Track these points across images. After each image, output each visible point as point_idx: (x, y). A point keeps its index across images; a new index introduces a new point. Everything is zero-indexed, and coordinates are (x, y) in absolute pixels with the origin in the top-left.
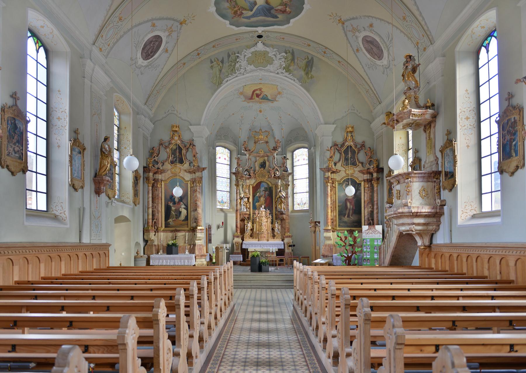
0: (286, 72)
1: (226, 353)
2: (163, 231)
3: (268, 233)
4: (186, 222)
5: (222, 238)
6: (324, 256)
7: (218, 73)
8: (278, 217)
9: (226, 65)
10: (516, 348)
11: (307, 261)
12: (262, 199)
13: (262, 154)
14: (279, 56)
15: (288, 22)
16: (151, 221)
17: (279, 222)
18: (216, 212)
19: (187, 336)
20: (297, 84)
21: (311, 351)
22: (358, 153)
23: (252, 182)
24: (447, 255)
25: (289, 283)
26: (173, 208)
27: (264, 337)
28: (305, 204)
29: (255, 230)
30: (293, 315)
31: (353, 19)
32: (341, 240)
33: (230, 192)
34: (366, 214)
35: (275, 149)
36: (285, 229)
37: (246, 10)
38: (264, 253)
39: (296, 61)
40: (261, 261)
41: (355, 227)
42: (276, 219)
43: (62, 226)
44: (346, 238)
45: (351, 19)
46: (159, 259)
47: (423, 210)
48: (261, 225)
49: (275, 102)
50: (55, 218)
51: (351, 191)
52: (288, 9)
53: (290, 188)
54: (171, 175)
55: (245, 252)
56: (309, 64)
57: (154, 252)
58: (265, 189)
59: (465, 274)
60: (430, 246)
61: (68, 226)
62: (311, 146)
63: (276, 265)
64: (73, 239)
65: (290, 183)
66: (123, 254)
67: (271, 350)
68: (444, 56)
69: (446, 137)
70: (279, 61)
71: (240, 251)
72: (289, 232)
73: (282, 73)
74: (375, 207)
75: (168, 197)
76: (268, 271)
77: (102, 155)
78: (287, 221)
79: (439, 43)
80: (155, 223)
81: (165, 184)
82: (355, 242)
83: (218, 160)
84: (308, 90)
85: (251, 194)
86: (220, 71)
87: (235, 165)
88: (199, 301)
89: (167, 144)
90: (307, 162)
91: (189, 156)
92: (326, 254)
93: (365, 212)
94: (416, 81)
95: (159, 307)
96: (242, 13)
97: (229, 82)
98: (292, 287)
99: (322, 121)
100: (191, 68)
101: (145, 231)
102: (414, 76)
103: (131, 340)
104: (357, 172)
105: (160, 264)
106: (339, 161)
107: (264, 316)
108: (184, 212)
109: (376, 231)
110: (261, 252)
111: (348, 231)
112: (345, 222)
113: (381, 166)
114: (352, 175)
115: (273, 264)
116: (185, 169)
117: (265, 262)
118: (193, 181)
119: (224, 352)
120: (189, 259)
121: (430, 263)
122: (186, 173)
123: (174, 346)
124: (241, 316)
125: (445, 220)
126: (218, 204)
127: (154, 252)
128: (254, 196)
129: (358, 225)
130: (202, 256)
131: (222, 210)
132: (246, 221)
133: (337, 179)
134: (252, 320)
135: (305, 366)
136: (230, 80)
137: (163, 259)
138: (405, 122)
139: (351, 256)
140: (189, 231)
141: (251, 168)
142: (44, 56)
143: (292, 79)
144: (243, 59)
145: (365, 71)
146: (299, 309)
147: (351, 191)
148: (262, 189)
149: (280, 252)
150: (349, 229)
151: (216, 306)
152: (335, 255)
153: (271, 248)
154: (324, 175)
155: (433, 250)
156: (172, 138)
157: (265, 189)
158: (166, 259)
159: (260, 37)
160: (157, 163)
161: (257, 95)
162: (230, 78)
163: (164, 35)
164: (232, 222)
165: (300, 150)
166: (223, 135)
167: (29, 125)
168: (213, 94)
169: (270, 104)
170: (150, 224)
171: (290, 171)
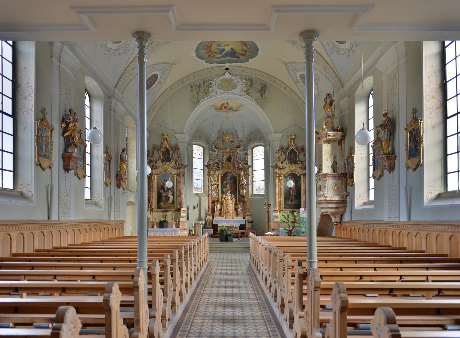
0: (246, 94)
1: (194, 321)
2: (157, 211)
3: (233, 213)
4: (172, 205)
5: (197, 216)
6: (273, 230)
7: (196, 95)
8: (240, 199)
9: (202, 89)
10: (363, 277)
11: (261, 232)
13: (228, 150)
14: (241, 83)
15: (248, 61)
17: (242, 204)
19: (172, 289)
20: (255, 103)
21: (276, 329)
22: (299, 154)
23: (220, 173)
24: (349, 229)
25: (247, 250)
26: (163, 195)
27: (229, 300)
29: (223, 210)
30: (248, 267)
31: (293, 63)
32: (285, 218)
33: (203, 180)
35: (238, 147)
37: (217, 53)
38: (229, 228)
39: (253, 86)
41: (297, 208)
42: (239, 201)
43: (101, 209)
44: (288, 216)
45: (291, 63)
46: (154, 231)
47: (334, 199)
49: (238, 112)
50: (96, 204)
51: (291, 184)
52: (247, 53)
55: (215, 227)
56: (263, 89)
57: (150, 226)
58: (230, 174)
59: (390, 246)
60: (340, 223)
61: (103, 209)
62: (266, 145)
63: (238, 237)
64: (106, 218)
65: (250, 174)
66: (130, 228)
67: (235, 310)
68: (349, 96)
70: (241, 86)
71: (211, 226)
72: (249, 211)
75: (160, 187)
77: (121, 161)
78: (247, 203)
79: (347, 87)
80: (150, 205)
81: (158, 177)
82: (295, 219)
83: (194, 156)
84: (262, 108)
85: (220, 182)
86: (198, 93)
87: (207, 159)
88: (172, 271)
89: (159, 148)
90: (263, 157)
91: (175, 156)
92: (275, 228)
94: (332, 111)
95: (139, 276)
96: (215, 56)
97: (204, 102)
98: (248, 252)
99: (273, 131)
102: (331, 108)
103: (115, 304)
104: (298, 168)
107: (229, 283)
110: (228, 227)
112: (289, 205)
115: (237, 236)
118: (178, 175)
119: (193, 320)
120: (176, 231)
121: (341, 235)
122: (172, 169)
123: (151, 309)
124: (214, 268)
125: (348, 204)
126: (194, 189)
128: (222, 184)
129: (298, 207)
130: (184, 229)
133: (283, 174)
134: (219, 287)
135: (266, 333)
137: (157, 231)
138: (324, 139)
139: (292, 229)
140: (175, 211)
141: (220, 161)
142: (89, 100)
146: (252, 263)
147: (291, 184)
148: (229, 178)
149: (242, 227)
150: (292, 210)
151: (187, 275)
154: (274, 171)
155: (342, 225)
156: (163, 143)
157: (230, 174)
158: (159, 231)
159: (227, 69)
161: (224, 107)
162: (205, 99)
163: (158, 73)
164: (205, 204)
166: (198, 136)
167: (86, 148)
169: (235, 113)
171: (250, 164)
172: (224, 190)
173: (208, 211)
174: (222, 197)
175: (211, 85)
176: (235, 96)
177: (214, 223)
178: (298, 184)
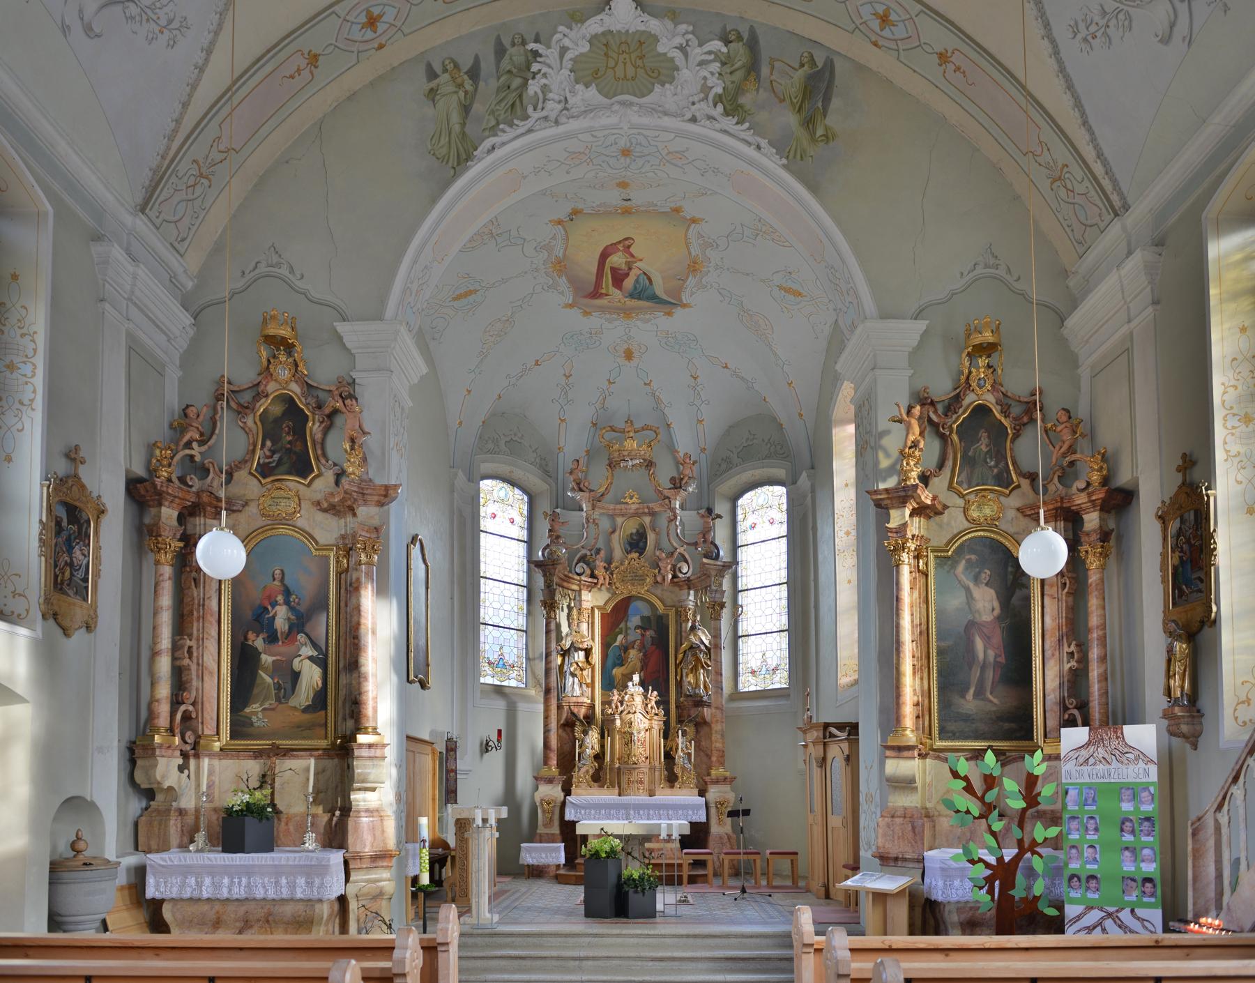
0: (727, 113)
3: (652, 769)
7: (455, 118)
8: (684, 713)
9: (489, 85)
12: (634, 655)
13: (633, 504)
14: (697, 53)
16: (164, 709)
17: (690, 730)
18: (478, 694)
20: (772, 162)
22: (1017, 436)
26: (266, 659)
28: (775, 670)
29: (608, 758)
34: (1053, 683)
36: (709, 757)
39: (765, 71)
40: (625, 873)
48: (628, 739)
49: (678, 312)
53: (726, 614)
54: (261, 521)
56: (818, 86)
65: (727, 599)
69: (1178, 478)
70: (698, 70)
71: (556, 830)
72: (722, 764)
73: (710, 118)
74: (1094, 653)
75: (248, 614)
76: (650, 913)
78: (717, 727)
80: (186, 717)
83: (485, 524)
84: (814, 188)
86: (466, 109)
87: (543, 539)
90: (784, 530)
92: (894, 851)
93: (1047, 677)
97: (499, 153)
100: (352, 97)
101: (137, 752)
104: (1011, 514)
105: (187, 894)
106: (941, 466)
108: (311, 675)
109: (1125, 752)
110: (626, 839)
111: (998, 753)
112: (967, 718)
113: (1123, 478)
114: (991, 523)
116: (319, 496)
117: (641, 878)
118: (347, 548)
122: (320, 516)
126: (486, 668)
127: (174, 838)
128: (606, 646)
129: (1015, 728)
131: (499, 690)
132: (578, 729)
136: (503, 144)
143: (749, 144)
144: (556, 64)
145: (1062, 70)
148: (635, 621)
149: (697, 836)
152: (934, 856)
153: (664, 823)
156: (266, 372)
158: (212, 871)
160: (204, 471)
164: (533, 731)
165: (759, 490)
168: (434, 200)
169: (661, 321)
170: (163, 721)
172: (617, 672)
173: (546, 761)
174: (606, 702)
175: (535, 67)
176: (667, 121)
177: (569, 815)
178: (1015, 600)
